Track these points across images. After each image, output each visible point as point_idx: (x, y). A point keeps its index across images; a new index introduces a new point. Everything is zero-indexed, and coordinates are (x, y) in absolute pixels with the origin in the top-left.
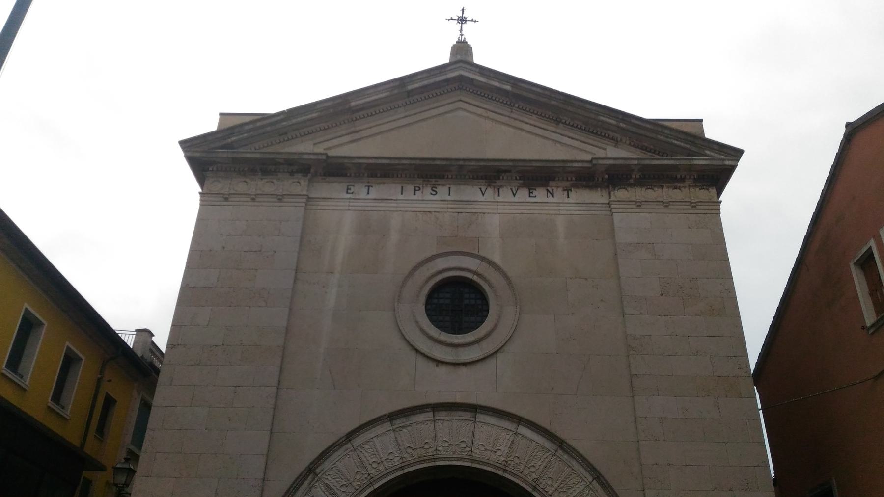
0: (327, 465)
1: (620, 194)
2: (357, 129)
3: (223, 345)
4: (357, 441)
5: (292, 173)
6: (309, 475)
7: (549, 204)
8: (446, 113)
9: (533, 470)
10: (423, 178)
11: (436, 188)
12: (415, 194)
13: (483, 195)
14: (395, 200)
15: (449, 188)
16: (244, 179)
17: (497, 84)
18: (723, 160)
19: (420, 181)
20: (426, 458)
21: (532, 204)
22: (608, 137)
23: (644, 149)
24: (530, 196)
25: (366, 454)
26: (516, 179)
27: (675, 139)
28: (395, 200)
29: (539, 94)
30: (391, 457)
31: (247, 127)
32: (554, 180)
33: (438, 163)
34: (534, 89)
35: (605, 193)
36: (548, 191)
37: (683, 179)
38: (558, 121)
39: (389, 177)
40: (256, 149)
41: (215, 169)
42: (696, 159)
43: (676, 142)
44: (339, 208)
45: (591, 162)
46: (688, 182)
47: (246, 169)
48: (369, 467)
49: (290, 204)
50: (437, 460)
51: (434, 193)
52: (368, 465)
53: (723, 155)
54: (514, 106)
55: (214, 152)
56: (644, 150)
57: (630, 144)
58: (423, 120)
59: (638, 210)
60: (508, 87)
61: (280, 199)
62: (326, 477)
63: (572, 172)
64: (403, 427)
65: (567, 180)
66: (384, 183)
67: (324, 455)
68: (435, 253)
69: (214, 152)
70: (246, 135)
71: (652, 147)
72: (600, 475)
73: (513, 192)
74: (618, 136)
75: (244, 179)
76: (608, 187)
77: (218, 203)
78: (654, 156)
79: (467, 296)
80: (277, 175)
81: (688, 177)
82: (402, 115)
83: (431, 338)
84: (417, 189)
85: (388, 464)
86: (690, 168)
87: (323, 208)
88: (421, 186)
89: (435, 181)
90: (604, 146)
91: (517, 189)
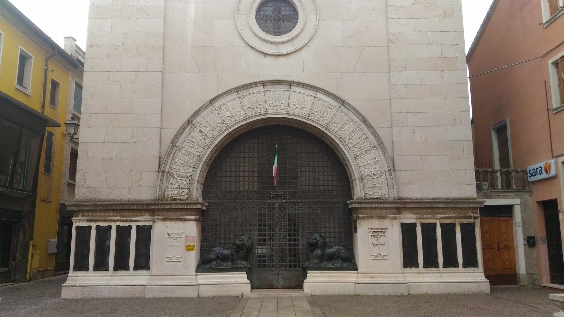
0: (199, 119)
4: (217, 104)
6: (188, 125)
9: (325, 118)
25: (223, 112)
62: (199, 126)
64: (245, 95)
67: (197, 113)
83: (260, 38)
85: (237, 118)
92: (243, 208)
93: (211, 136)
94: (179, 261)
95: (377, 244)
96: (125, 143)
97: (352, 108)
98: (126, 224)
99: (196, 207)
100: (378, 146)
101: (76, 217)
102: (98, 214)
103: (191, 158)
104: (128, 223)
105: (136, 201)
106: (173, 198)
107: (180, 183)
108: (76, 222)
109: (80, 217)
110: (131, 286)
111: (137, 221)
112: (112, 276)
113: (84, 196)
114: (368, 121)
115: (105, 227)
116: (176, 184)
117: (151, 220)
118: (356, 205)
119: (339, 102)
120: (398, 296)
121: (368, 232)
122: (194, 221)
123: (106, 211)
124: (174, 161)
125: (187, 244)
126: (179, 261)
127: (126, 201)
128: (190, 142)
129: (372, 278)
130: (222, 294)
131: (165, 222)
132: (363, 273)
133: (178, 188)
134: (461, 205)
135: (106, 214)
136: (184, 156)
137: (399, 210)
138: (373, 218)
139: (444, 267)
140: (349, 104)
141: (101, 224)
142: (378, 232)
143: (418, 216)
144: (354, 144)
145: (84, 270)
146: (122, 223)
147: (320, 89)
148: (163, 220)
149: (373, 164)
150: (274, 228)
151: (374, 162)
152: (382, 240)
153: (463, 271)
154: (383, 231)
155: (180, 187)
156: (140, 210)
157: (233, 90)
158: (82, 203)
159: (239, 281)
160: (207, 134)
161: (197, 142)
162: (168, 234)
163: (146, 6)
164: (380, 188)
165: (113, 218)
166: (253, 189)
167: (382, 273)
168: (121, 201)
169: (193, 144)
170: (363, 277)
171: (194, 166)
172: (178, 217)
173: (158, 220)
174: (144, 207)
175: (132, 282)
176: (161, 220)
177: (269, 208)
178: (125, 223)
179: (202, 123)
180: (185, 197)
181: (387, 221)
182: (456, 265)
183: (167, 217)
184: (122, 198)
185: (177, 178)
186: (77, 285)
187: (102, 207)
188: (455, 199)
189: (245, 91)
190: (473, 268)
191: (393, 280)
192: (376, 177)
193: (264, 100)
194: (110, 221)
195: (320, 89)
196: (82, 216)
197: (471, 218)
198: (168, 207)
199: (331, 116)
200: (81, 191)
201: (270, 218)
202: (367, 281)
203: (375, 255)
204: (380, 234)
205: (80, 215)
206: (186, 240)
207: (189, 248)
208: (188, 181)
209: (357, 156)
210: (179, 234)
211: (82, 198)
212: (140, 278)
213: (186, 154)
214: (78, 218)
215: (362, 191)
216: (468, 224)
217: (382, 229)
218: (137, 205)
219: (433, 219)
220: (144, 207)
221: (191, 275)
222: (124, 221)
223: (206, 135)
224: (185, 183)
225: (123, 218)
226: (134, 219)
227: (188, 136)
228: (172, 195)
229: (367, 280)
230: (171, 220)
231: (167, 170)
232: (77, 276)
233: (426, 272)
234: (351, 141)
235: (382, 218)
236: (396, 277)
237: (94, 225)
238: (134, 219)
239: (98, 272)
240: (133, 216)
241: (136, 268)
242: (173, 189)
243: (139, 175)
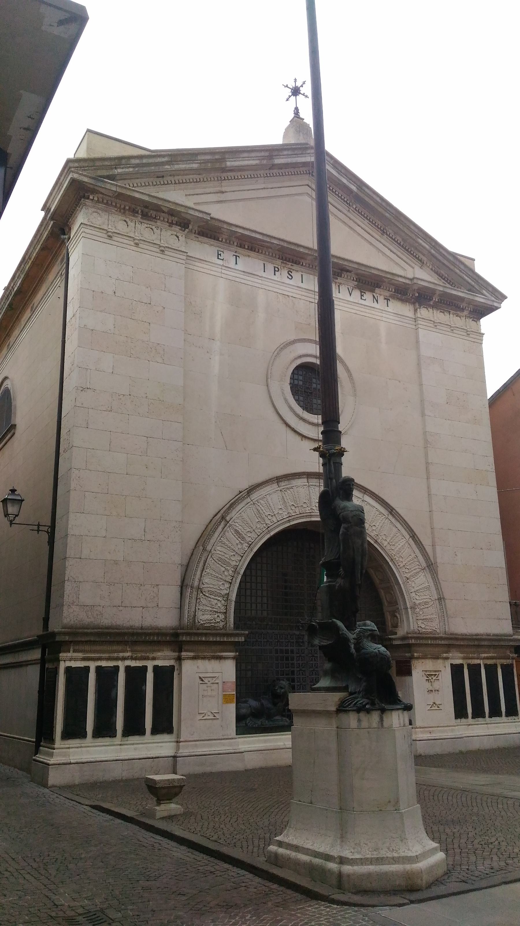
0: (233, 514)
1: (424, 312)
2: (223, 189)
3: (130, 395)
4: (255, 496)
5: (171, 224)
6: (221, 522)
7: (375, 310)
8: (296, 194)
9: (374, 528)
10: (282, 259)
11: (291, 273)
12: (275, 275)
13: (350, 295)
14: (260, 277)
15: (302, 275)
16: (125, 218)
17: (345, 181)
18: (493, 301)
19: (279, 262)
20: (305, 514)
21: (363, 307)
22: (418, 259)
23: (441, 276)
24: (361, 299)
25: (263, 508)
26: (353, 280)
27: (465, 275)
28: (260, 277)
29: (380, 205)
30: (305, 506)
31: (133, 161)
32: (380, 287)
33: (302, 250)
34: (374, 196)
35: (411, 307)
36: (374, 296)
37: (463, 310)
38: (384, 232)
39: (255, 251)
40: (133, 186)
41: (96, 199)
42: (478, 296)
43: (466, 278)
44: (212, 273)
45: (411, 280)
46: (466, 313)
47: (127, 208)
48: (266, 518)
49: (171, 258)
50: (312, 516)
51: (290, 277)
52: (265, 517)
53: (493, 297)
54: (352, 206)
55: (103, 181)
56: (440, 276)
57: (432, 269)
58: (371, 244)
59: (434, 330)
60: (354, 188)
61: (163, 251)
62: (235, 524)
63: (393, 284)
64: (287, 488)
65: (389, 290)
66: (249, 256)
67: (232, 505)
68: (292, 338)
69: (103, 181)
70: (131, 170)
71: (446, 275)
72: (415, 534)
73: (349, 292)
74: (424, 259)
75: (125, 218)
76: (414, 303)
77: (102, 240)
78: (445, 284)
79: (314, 380)
80: (156, 222)
81: (467, 308)
82: (263, 186)
83: (298, 416)
84: (276, 269)
85: (279, 518)
86: (470, 302)
87: (199, 269)
88: (279, 268)
89: (291, 265)
90: (413, 265)
91: (352, 289)
92: (288, 642)
93: (250, 539)
94: (215, 718)
95: (432, 691)
96: (135, 540)
97: (401, 519)
98: (111, 664)
99: (238, 640)
100: (427, 568)
101: (65, 652)
102: (105, 647)
103: (226, 569)
104: (141, 662)
105: (151, 629)
106: (205, 625)
107: (213, 604)
108: (65, 661)
109: (71, 652)
110: (152, 758)
111: (154, 659)
112: (121, 745)
113: (76, 620)
114: (417, 536)
115: (110, 668)
116: (209, 605)
117: (173, 657)
118: (413, 641)
119: (387, 510)
120: (457, 754)
121: (423, 676)
122: (232, 660)
123: (111, 643)
124: (206, 572)
125: (225, 693)
126: (215, 718)
127: (138, 628)
128: (225, 546)
129: (430, 733)
130: (270, 763)
131: (195, 661)
132: (421, 728)
133: (211, 611)
134: (502, 643)
135: (110, 648)
136: (218, 565)
137: (449, 647)
138: (427, 658)
139: (473, 718)
140: (398, 513)
141: (104, 664)
142: (432, 675)
143: (465, 655)
144: (404, 563)
145: (80, 738)
146: (134, 661)
147: (368, 491)
148: (194, 658)
149: (423, 590)
150: (303, 671)
151: (424, 587)
152: (436, 685)
153: (506, 721)
154: (436, 674)
155: (214, 609)
156: (159, 643)
157: (274, 480)
158: (80, 631)
159: (280, 744)
160: (244, 536)
161: (233, 547)
162: (200, 678)
163: (160, 345)
164: (431, 620)
165: (121, 655)
166: (262, 614)
167: (438, 727)
168: (131, 627)
169: (228, 548)
170: (422, 732)
171: (230, 581)
172: (214, 654)
173: (187, 657)
174: (168, 638)
175: (149, 753)
176: (81, 659)
177: (297, 642)
178: (138, 661)
179: (238, 521)
180: (221, 624)
181: (440, 661)
182: (499, 715)
183: (200, 654)
184: (131, 623)
185: (210, 596)
186: (72, 761)
187: (109, 638)
188: (497, 635)
189: (286, 483)
190: (514, 717)
191: (450, 735)
192: (427, 606)
193: (309, 497)
194: (117, 659)
195: (368, 491)
196: (74, 651)
197: (509, 659)
198: (204, 639)
199: (380, 526)
200: (71, 610)
201: (299, 656)
202: (104, 757)
203: (430, 705)
204: (434, 678)
205: (71, 650)
206: (223, 688)
207: (226, 699)
208: (223, 602)
209: (408, 579)
210: (214, 679)
211: (74, 621)
212: (161, 747)
213: (220, 563)
214: (69, 655)
215: (415, 623)
216: (490, 665)
217: (436, 671)
218: (153, 634)
219: (478, 659)
220: (168, 638)
221: (233, 738)
222: (136, 659)
223: (243, 538)
224: (219, 605)
225: (137, 654)
226: (151, 655)
227: (221, 537)
228: (203, 621)
229: (427, 736)
230: (204, 658)
231: (196, 584)
232: (69, 748)
233: (474, 723)
234: (401, 559)
235: (434, 658)
236: (452, 731)
237: (93, 665)
238: (151, 655)
239: (100, 739)
240: (146, 652)
241: (155, 731)
242: (206, 613)
243: (155, 589)
